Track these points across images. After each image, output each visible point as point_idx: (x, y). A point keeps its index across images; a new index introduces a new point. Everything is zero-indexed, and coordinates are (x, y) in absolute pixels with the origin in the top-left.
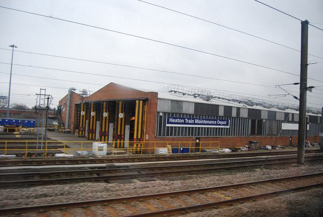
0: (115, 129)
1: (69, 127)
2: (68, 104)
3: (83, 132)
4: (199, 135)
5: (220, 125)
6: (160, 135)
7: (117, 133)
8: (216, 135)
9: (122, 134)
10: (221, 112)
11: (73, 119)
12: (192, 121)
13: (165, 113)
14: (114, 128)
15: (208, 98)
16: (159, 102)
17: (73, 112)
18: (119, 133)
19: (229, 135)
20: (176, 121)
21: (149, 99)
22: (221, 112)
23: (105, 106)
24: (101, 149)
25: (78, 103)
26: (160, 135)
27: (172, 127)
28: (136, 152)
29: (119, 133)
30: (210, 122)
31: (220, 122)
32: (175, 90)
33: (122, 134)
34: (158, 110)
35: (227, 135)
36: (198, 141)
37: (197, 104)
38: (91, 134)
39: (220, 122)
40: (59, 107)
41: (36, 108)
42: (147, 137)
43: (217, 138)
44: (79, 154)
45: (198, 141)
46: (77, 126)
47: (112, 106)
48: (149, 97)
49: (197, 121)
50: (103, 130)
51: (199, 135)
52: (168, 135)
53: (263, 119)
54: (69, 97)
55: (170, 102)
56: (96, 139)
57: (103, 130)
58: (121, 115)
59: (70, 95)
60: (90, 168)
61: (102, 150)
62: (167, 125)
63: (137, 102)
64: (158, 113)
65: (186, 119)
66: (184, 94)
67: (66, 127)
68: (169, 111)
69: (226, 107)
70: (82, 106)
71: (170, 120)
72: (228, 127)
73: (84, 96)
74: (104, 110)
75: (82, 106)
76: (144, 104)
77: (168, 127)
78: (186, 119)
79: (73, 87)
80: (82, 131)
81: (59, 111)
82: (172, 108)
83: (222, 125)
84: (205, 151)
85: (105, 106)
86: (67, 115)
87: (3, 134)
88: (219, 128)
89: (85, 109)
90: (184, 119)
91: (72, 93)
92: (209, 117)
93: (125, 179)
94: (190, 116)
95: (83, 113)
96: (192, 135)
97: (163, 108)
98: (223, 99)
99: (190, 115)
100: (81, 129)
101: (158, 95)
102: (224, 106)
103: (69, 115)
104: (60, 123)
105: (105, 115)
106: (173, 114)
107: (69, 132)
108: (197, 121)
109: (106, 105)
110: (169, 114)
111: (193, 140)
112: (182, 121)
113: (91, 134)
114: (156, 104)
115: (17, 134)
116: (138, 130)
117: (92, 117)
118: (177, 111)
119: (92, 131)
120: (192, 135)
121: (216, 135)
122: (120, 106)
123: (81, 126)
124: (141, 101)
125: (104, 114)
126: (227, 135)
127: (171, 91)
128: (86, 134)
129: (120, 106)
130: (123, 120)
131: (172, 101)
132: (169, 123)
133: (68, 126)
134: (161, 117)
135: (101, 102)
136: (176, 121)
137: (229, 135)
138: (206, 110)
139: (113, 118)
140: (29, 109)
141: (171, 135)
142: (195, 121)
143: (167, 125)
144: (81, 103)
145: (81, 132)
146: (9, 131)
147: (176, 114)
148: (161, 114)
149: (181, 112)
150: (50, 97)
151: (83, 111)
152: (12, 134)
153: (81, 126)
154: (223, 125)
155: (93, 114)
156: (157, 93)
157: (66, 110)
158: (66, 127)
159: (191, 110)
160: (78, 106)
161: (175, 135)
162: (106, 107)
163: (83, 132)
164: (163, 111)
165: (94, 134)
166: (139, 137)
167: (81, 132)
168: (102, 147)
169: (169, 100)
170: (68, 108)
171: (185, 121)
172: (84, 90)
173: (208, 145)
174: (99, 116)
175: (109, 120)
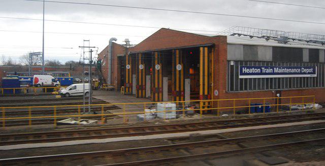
0: (153, 82)
1: (112, 83)
2: (109, 57)
3: (130, 89)
4: (279, 88)
5: (305, 73)
6: (232, 89)
7: (154, 86)
8: (301, 87)
9: (182, 89)
10: (306, 57)
11: (116, 74)
12: (270, 70)
13: (236, 62)
14: (151, 82)
15: (285, 40)
16: (229, 47)
17: (116, 66)
18: (156, 86)
19: (317, 86)
20: (251, 71)
21: (216, 45)
22: (306, 57)
23: (156, 57)
24: (168, 110)
25: (123, 55)
26: (232, 89)
27: (246, 79)
28: (210, 112)
29: (156, 86)
30: (293, 71)
31: (305, 70)
32: (240, 32)
33: (144, 84)
34: (229, 58)
35: (314, 86)
36: (278, 95)
37: (274, 48)
38: (140, 91)
39: (305, 70)
40: (99, 60)
41: (67, 64)
42: (216, 93)
43: (302, 90)
44: (142, 119)
45: (278, 95)
46: (122, 82)
47: (167, 57)
48: (215, 42)
49: (276, 70)
50: (140, 84)
51: (279, 88)
52: (241, 89)
53: (229, 61)
54: (109, 50)
55: (242, 47)
56: (147, 96)
57: (140, 84)
58: (179, 67)
59: (112, 47)
60: (172, 140)
61: (170, 112)
62: (241, 77)
63: (201, 49)
64: (229, 61)
65: (263, 68)
66: (251, 37)
67: (109, 83)
68: (242, 59)
69: (311, 50)
70: (127, 58)
71: (244, 70)
72: (315, 76)
73: (128, 47)
74: (156, 61)
75: (127, 58)
76: (209, 52)
77: (241, 79)
78: (263, 68)
79: (113, 37)
80: (129, 88)
81: (99, 66)
82: (245, 54)
83: (307, 74)
84: (288, 109)
85: (156, 57)
86: (109, 71)
87: (42, 95)
88: (304, 78)
89: (130, 62)
90: (260, 68)
91: (113, 45)
92: (290, 65)
93: (226, 157)
94: (268, 64)
95: (128, 67)
96: (271, 88)
97: (233, 55)
98: (299, 40)
99: (268, 62)
100: (128, 85)
101: (228, 40)
102: (273, 47)
103: (111, 70)
104: (100, 79)
105: (158, 67)
106: (246, 62)
107: (112, 90)
108: (276, 70)
109: (158, 55)
110: (241, 62)
111: (273, 95)
112: (258, 71)
113: (140, 91)
114: (226, 51)
115: (57, 94)
116: (204, 85)
117: (177, 73)
118: (251, 59)
119: (141, 88)
120: (271, 88)
121: (301, 87)
122: (177, 56)
123: (127, 82)
124: (206, 49)
125: (156, 67)
126: (314, 86)
127: (234, 34)
128: (134, 92)
129: (177, 56)
130: (182, 73)
131: (244, 45)
132: (242, 74)
133: (111, 82)
134: (232, 66)
135: (172, 50)
136: (251, 71)
137: (317, 86)
138: (286, 54)
139: (168, 69)
140: (62, 66)
141: (246, 89)
142: (273, 70)
143: (241, 77)
144: (125, 56)
145: (127, 89)
146: (47, 92)
147: (251, 61)
148: (232, 63)
149: (256, 60)
150: (93, 49)
151: (129, 64)
152: (50, 94)
153: (127, 82)
154: (309, 73)
155: (141, 67)
156: (225, 37)
157: (107, 64)
158: (109, 83)
159: (268, 56)
160: (122, 61)
161: (250, 88)
162: (158, 58)
163: (130, 89)
164: (235, 59)
165: (160, 94)
166: (206, 93)
167: (127, 89)
168: (171, 108)
169: (241, 45)
170: (109, 62)
171: (261, 70)
172: (126, 39)
173: (288, 101)
174: (135, 69)
175: (145, 73)
